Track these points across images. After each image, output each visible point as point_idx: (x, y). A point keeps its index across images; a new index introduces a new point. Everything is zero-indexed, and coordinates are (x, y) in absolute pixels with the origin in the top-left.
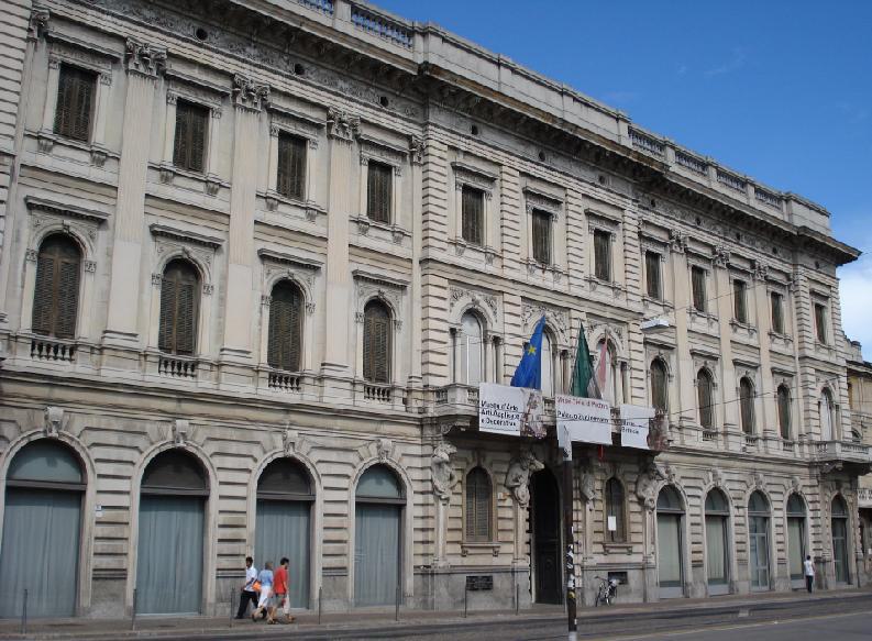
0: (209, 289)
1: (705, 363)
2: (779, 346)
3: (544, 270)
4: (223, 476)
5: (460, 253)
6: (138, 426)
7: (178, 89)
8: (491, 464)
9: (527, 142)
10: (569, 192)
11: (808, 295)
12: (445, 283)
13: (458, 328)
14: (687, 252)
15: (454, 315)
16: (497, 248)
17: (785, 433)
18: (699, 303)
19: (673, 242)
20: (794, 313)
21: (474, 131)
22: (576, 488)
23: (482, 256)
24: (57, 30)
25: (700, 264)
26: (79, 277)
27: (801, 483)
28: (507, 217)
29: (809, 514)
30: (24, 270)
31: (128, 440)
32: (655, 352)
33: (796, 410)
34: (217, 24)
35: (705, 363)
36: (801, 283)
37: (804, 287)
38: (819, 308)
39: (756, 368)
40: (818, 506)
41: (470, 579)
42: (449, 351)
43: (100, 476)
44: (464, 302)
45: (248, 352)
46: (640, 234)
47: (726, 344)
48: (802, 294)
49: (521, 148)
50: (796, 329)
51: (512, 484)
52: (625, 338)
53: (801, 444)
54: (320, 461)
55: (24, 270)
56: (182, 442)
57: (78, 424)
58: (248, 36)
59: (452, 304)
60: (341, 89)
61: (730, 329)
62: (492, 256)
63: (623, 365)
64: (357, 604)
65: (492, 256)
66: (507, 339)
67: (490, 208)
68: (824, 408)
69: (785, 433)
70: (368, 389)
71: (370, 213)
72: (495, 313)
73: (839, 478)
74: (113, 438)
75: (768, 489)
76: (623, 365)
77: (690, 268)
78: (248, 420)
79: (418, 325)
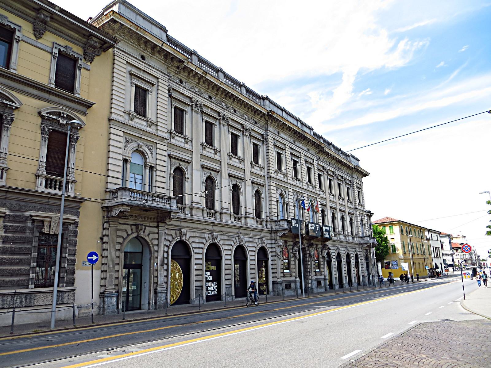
0: (242, 193)
1: (258, 188)
2: (256, 170)
3: (297, 180)
4: (196, 251)
5: (132, 119)
6: (203, 235)
7: (135, 80)
8: (148, 235)
9: (290, 137)
10: (286, 146)
11: (273, 147)
12: (121, 134)
13: (129, 159)
14: (229, 125)
15: (128, 153)
16: (154, 119)
17: (258, 215)
18: (235, 150)
19: (194, 104)
20: (265, 153)
21: (278, 133)
22: (308, 254)
23: (145, 123)
24: (174, 94)
25: (235, 132)
26: (240, 198)
27: (266, 242)
28: (159, 106)
29: (360, 261)
30: (170, 180)
31: (201, 240)
32: (176, 164)
33: (354, 226)
34: (214, 94)
35: (258, 188)
36: (269, 140)
37: (355, 184)
38: (359, 192)
39: (218, 172)
40: (362, 258)
41: (286, 285)
42: (120, 169)
43: (196, 253)
44: (134, 145)
45: (200, 203)
46: (170, 96)
47: (248, 173)
48: (270, 145)
49: (289, 139)
50: (266, 163)
51: (294, 252)
52: (154, 153)
53: (356, 237)
54: (193, 242)
55: (170, 180)
56: (216, 240)
57: (190, 237)
58: (222, 98)
59: (125, 146)
60: (196, 91)
61: (227, 157)
62: (150, 123)
63: (287, 204)
64: (236, 297)
65: (150, 123)
66: (158, 168)
67: (151, 99)
68: (280, 205)
69: (258, 215)
70: (235, 218)
71: (207, 142)
72: (152, 154)
73: (287, 239)
74: (197, 240)
75: (247, 244)
76: (151, 168)
77: (276, 152)
78: (192, 228)
79: (268, 199)
